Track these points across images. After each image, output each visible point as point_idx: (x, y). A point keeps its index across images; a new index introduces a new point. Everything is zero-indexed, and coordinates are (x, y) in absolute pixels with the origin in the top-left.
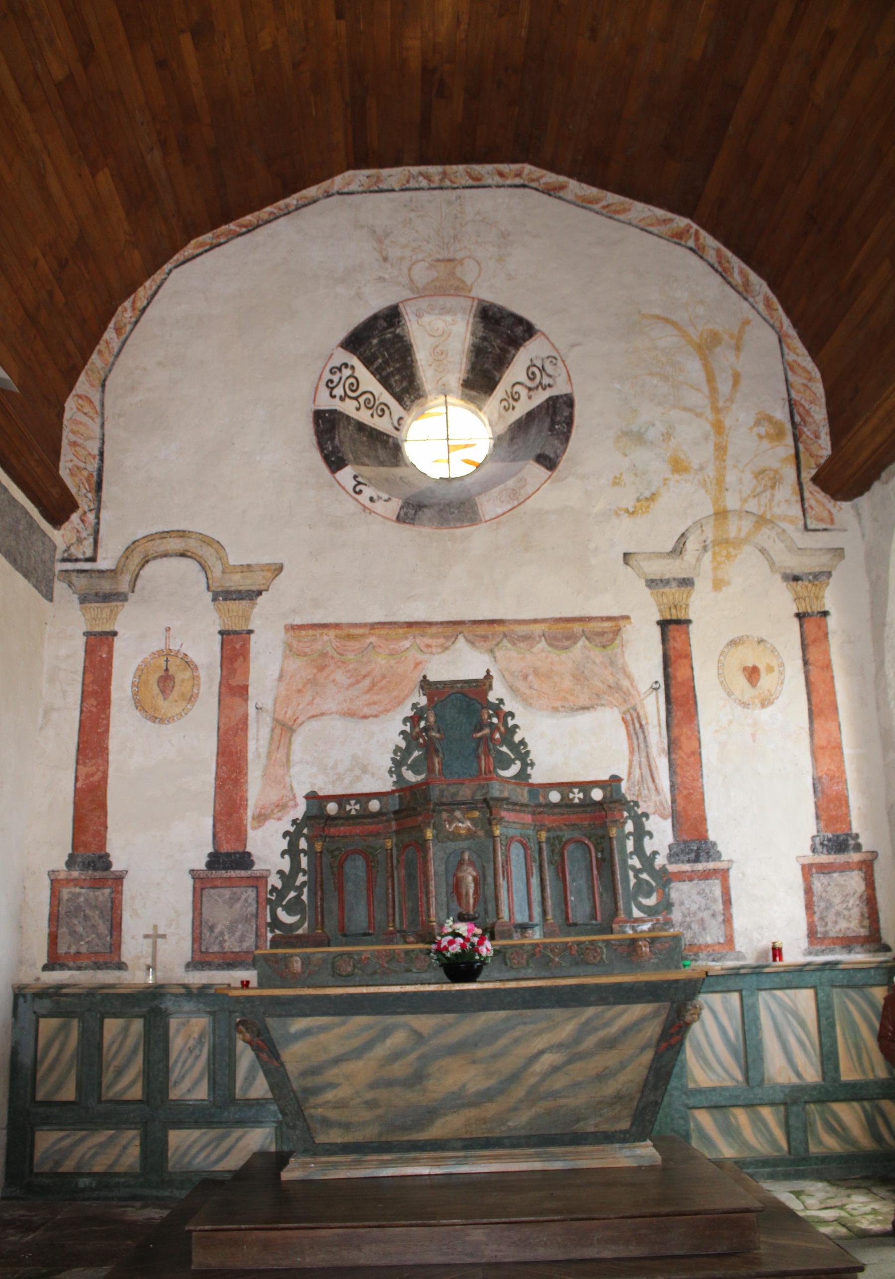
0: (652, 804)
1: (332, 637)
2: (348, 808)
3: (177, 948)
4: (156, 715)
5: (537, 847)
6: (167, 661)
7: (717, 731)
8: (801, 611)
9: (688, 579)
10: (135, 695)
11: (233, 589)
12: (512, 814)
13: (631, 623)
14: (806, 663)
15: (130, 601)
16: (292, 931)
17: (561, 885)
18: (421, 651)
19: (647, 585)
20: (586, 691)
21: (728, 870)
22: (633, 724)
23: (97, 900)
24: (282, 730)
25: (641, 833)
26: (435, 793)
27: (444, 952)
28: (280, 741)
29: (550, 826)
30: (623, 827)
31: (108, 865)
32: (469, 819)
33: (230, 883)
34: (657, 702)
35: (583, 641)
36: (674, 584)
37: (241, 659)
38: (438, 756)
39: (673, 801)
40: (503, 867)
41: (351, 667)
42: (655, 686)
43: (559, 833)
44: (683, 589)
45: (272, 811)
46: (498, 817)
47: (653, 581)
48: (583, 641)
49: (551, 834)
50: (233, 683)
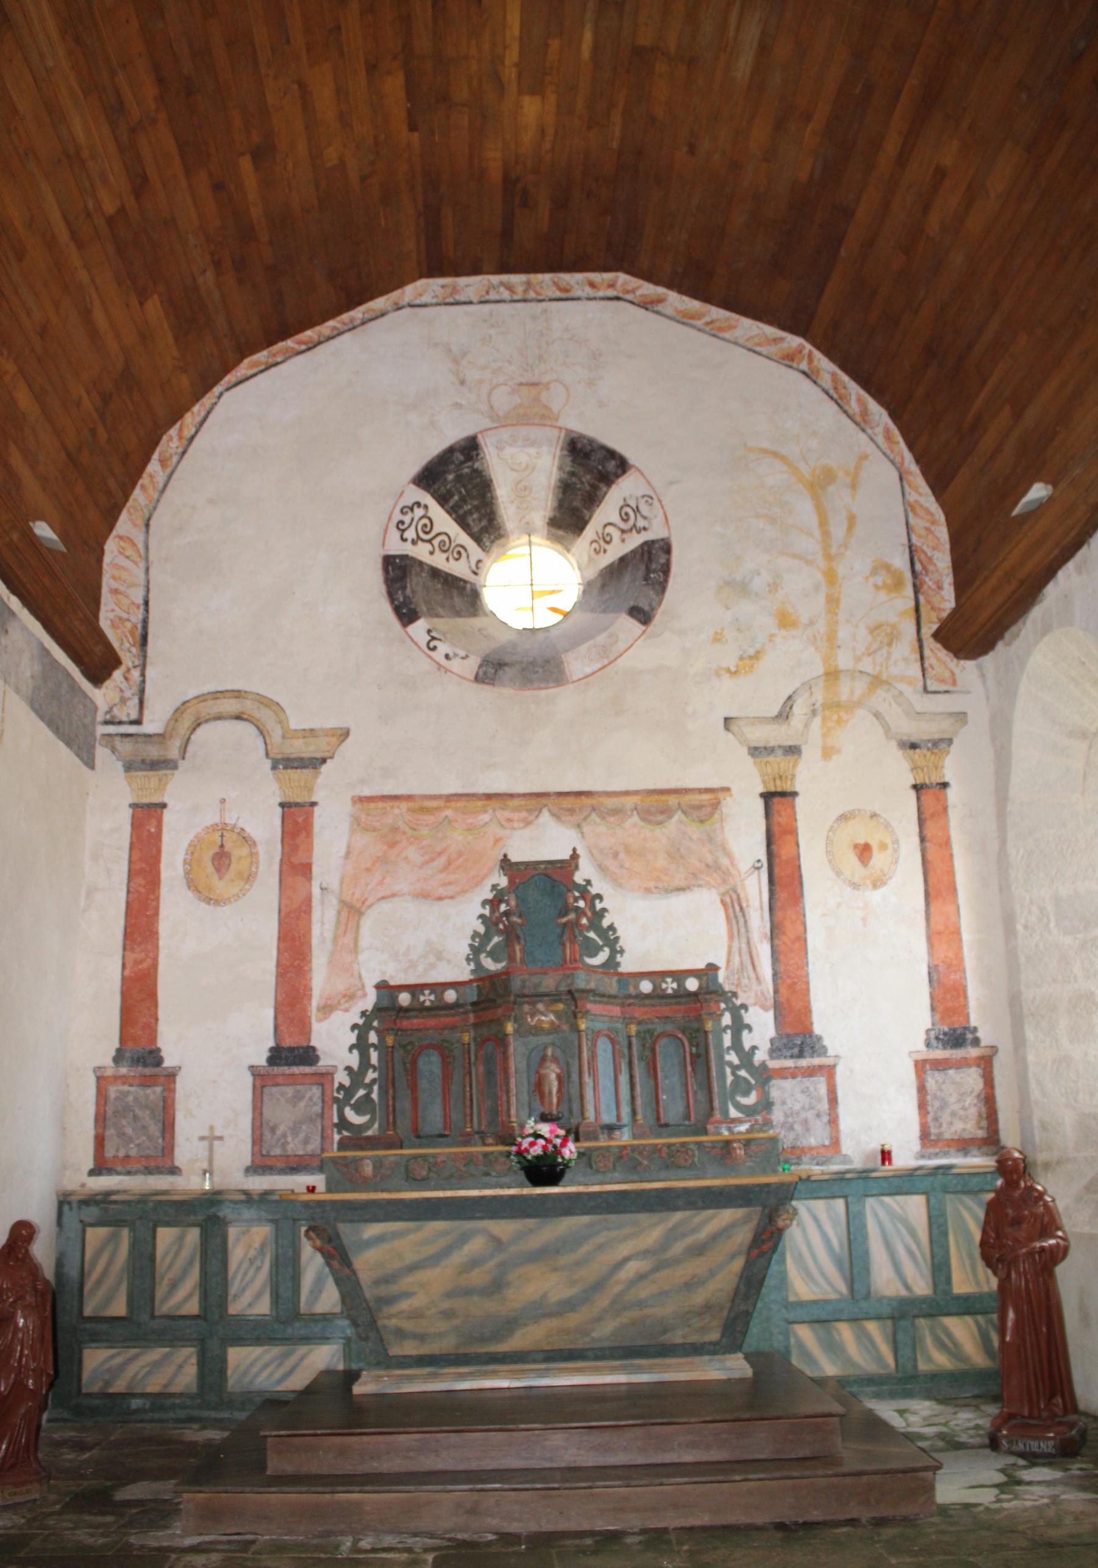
0: (752, 994)
1: (404, 810)
5: (625, 1043)
6: (222, 836)
9: (795, 747)
10: (187, 873)
12: (600, 1006)
14: (923, 839)
17: (652, 1082)
18: (502, 826)
21: (834, 1066)
22: (733, 906)
25: (739, 1027)
26: (516, 984)
27: (525, 1154)
30: (720, 1020)
31: (159, 1061)
32: (552, 1012)
33: (292, 1080)
34: (760, 883)
35: (678, 816)
36: (779, 752)
37: (304, 833)
38: (519, 943)
39: (776, 991)
41: (424, 843)
42: (757, 865)
43: (650, 1026)
47: (756, 748)
48: (678, 816)
49: (643, 1028)
50: (296, 860)
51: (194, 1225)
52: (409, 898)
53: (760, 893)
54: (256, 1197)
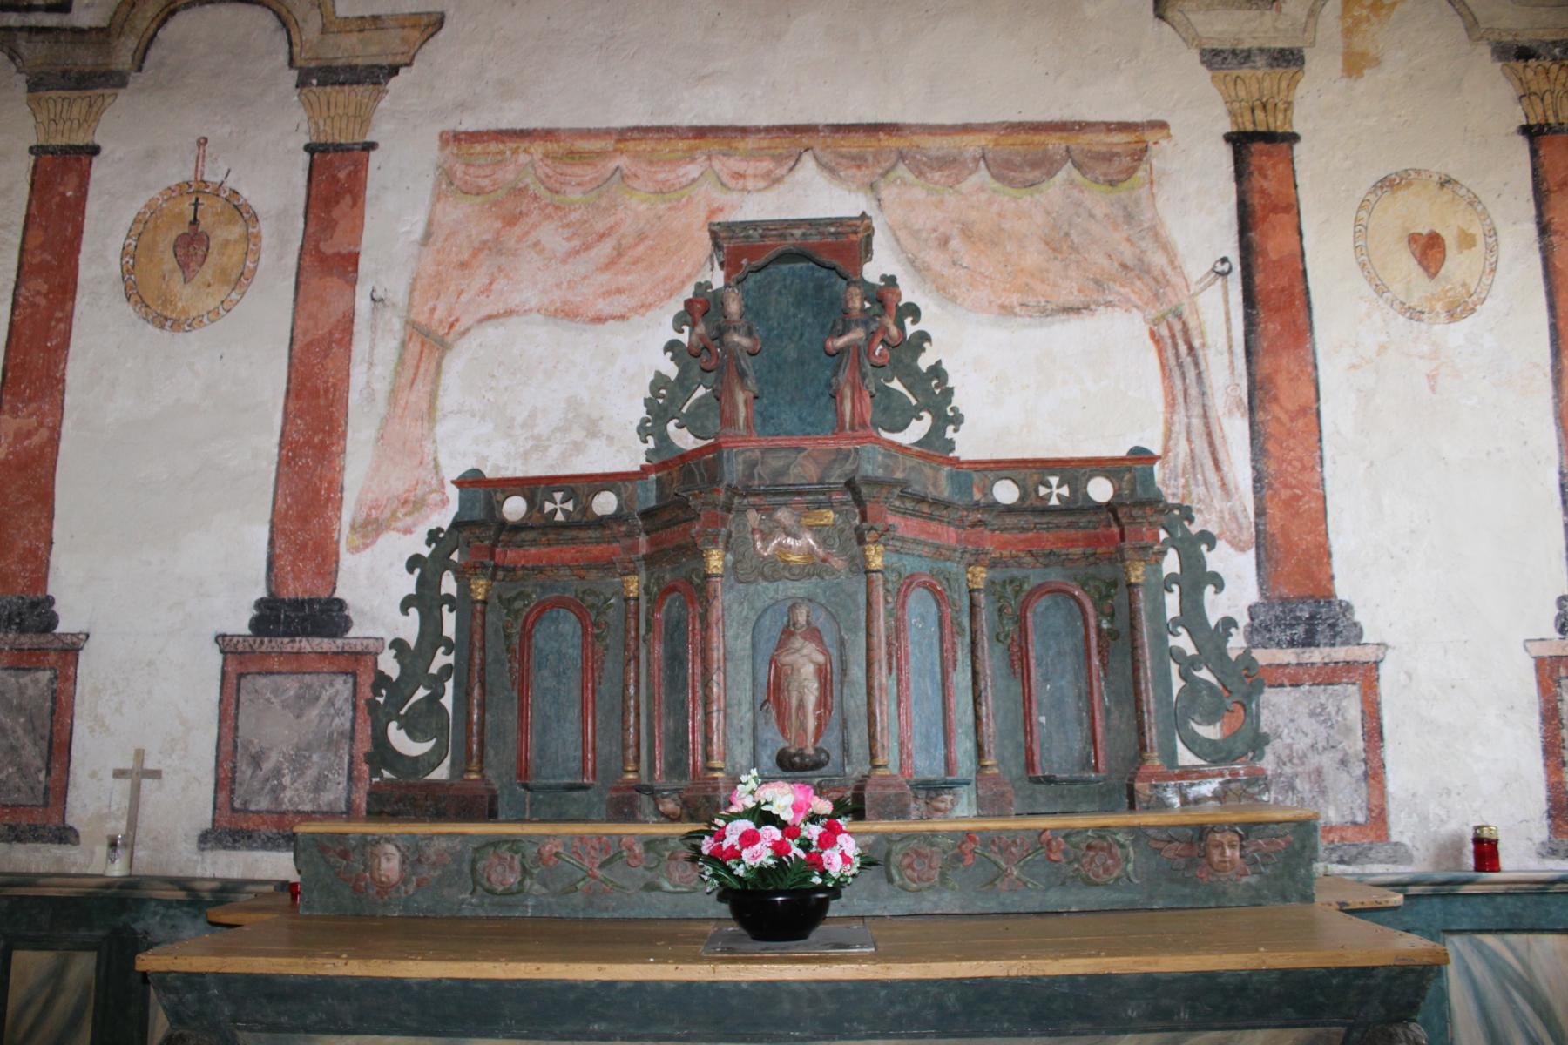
0: (1214, 517)
1: (538, 157)
2: (549, 506)
3: (183, 800)
4: (167, 313)
5: (966, 601)
6: (196, 204)
7: (1353, 367)
8: (1533, 122)
9: (1291, 51)
10: (126, 272)
11: (340, 63)
12: (913, 522)
13: (1169, 136)
14: (1544, 229)
15: (130, 86)
16: (416, 773)
17: (1016, 688)
18: (723, 184)
19: (1203, 62)
20: (1072, 273)
21: (1377, 663)
22: (1175, 345)
23: (22, 693)
24: (423, 344)
25: (1196, 579)
26: (734, 471)
27: (731, 863)
28: (418, 367)
29: (996, 555)
30: (1158, 563)
31: (50, 622)
32: (810, 528)
33: (297, 664)
34: (1226, 302)
35: (1067, 172)
36: (1260, 61)
37: (348, 198)
38: (744, 388)
39: (1260, 512)
40: (889, 644)
41: (574, 216)
42: (1220, 268)
43: (1016, 572)
44: (1280, 70)
45: (394, 513)
46: (880, 526)
47: (1216, 53)
48: (1067, 172)
49: (1000, 574)
50: (328, 248)
51: (86, 947)
52: (540, 317)
53: (1228, 320)
54: (207, 897)
